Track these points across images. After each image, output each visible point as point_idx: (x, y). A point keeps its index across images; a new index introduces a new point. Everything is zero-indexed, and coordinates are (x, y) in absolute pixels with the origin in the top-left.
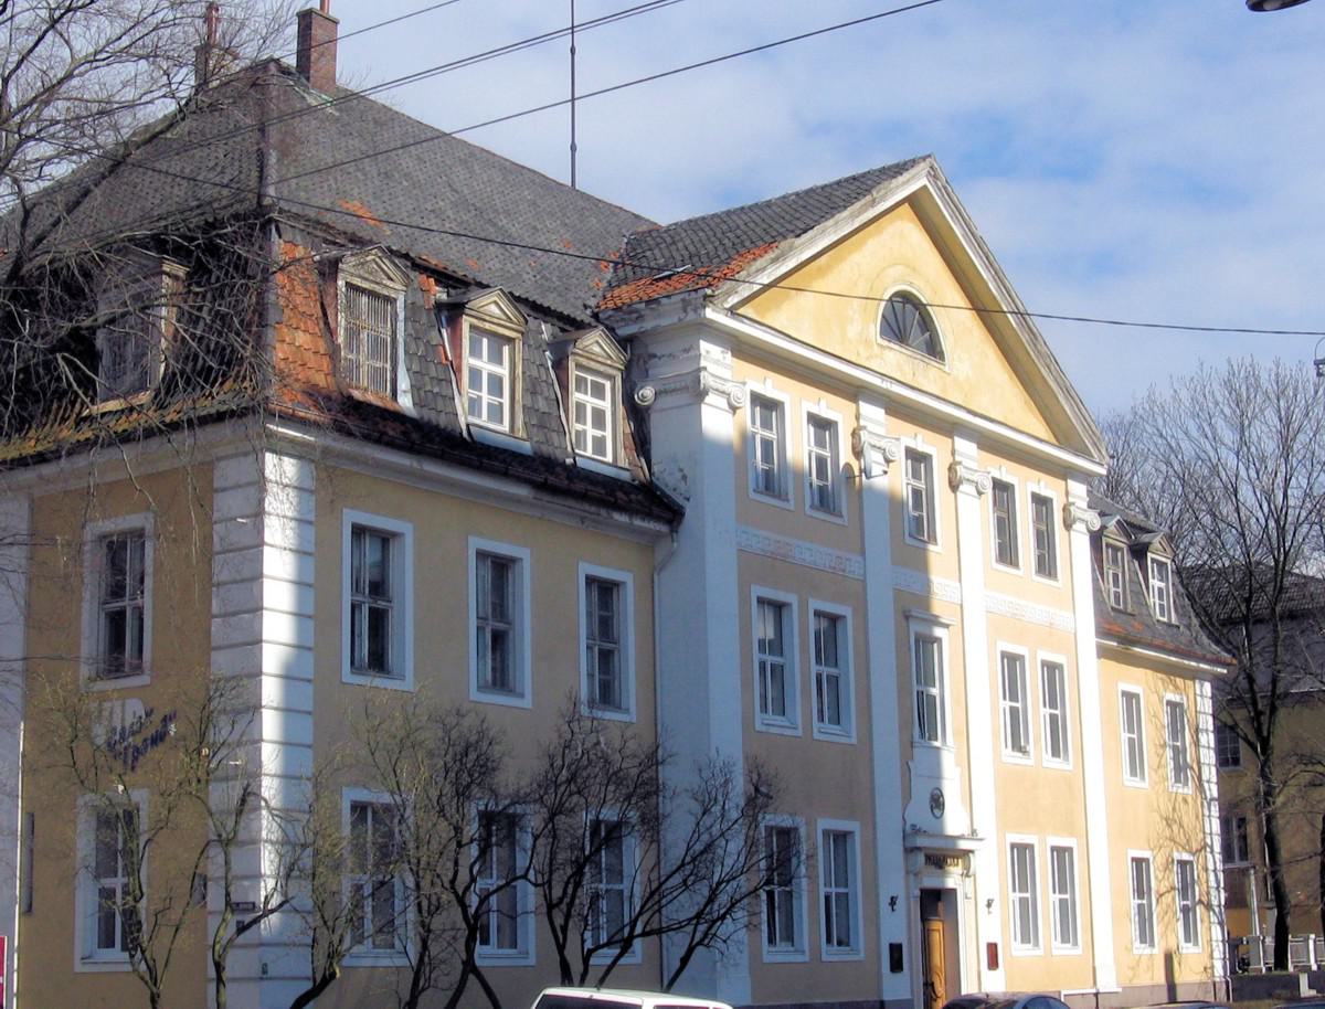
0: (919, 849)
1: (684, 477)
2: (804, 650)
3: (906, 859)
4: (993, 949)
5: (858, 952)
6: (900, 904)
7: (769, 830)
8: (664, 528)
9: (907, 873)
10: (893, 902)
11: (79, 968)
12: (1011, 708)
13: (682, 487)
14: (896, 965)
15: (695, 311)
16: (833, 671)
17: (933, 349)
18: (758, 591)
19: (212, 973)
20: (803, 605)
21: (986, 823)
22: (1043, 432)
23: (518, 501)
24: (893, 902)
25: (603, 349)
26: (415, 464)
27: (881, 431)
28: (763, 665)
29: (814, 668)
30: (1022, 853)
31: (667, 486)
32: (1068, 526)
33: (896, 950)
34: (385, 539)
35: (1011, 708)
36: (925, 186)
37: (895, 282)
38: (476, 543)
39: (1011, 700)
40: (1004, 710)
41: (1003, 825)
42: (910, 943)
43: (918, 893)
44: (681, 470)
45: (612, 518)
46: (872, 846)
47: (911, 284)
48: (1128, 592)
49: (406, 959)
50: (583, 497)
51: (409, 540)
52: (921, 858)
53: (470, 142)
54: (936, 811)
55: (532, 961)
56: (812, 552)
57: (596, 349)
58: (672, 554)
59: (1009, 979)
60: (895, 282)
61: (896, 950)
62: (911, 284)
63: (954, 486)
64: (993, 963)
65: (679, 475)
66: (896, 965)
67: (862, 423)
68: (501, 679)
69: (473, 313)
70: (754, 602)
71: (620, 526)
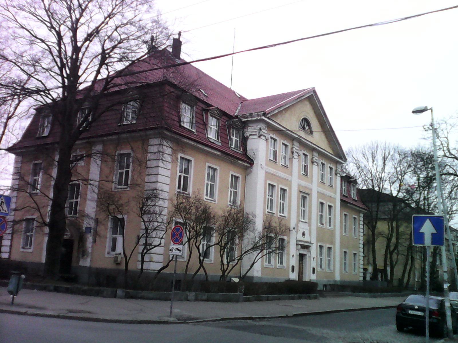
0: (299, 244)
1: (254, 154)
2: (277, 196)
3: (296, 246)
6: (294, 256)
7: (279, 238)
9: (296, 249)
10: (293, 256)
11: (106, 256)
12: (271, 199)
13: (254, 156)
14: (293, 271)
15: (260, 117)
17: (311, 132)
18: (269, 182)
19: (140, 259)
20: (278, 186)
21: (314, 241)
22: (331, 152)
24: (314, 258)
25: (217, 112)
26: (196, 144)
29: (279, 201)
30: (321, 247)
31: (250, 156)
32: (336, 174)
36: (312, 94)
37: (304, 116)
38: (231, 173)
39: (303, 207)
41: (318, 240)
43: (298, 254)
44: (254, 153)
50: (181, 136)
52: (300, 246)
54: (304, 237)
55: (212, 262)
56: (282, 174)
57: (215, 112)
58: (251, 172)
64: (314, 272)
65: (253, 154)
66: (293, 271)
68: (330, 226)
69: (211, 112)
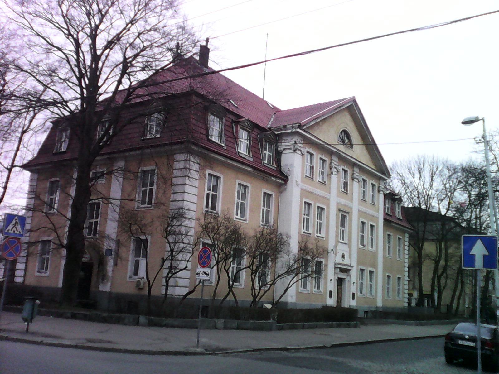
2: (314, 215)
3: (335, 270)
4: (354, 294)
5: (241, 285)
6: (355, 284)
8: (283, 182)
10: (331, 280)
12: (307, 218)
13: (288, 172)
14: (331, 296)
16: (344, 229)
17: (351, 146)
18: (305, 200)
21: (354, 264)
23: (249, 172)
26: (225, 160)
27: (337, 164)
28: (317, 222)
30: (362, 271)
32: (379, 191)
33: (331, 292)
34: (246, 187)
35: (307, 218)
36: (352, 104)
37: (343, 128)
40: (304, 219)
42: (334, 291)
43: (337, 278)
45: (271, 178)
46: (377, 272)
47: (346, 128)
48: (223, 129)
49: (269, 281)
51: (222, 179)
52: (338, 270)
53: (226, 76)
54: (343, 259)
58: (285, 189)
59: (357, 302)
60: (343, 128)
61: (331, 292)
62: (346, 128)
63: (353, 179)
64: (353, 298)
66: (331, 296)
67: (354, 172)
68: (372, 247)
70: (317, 207)
71: (273, 181)
